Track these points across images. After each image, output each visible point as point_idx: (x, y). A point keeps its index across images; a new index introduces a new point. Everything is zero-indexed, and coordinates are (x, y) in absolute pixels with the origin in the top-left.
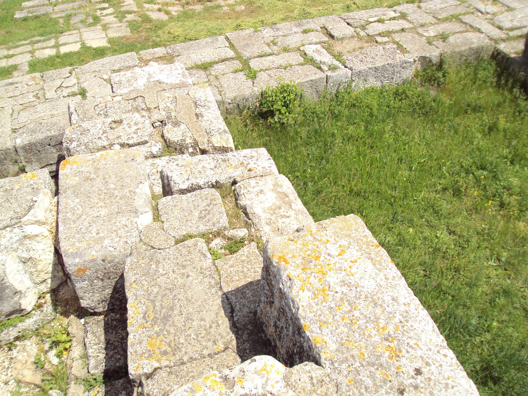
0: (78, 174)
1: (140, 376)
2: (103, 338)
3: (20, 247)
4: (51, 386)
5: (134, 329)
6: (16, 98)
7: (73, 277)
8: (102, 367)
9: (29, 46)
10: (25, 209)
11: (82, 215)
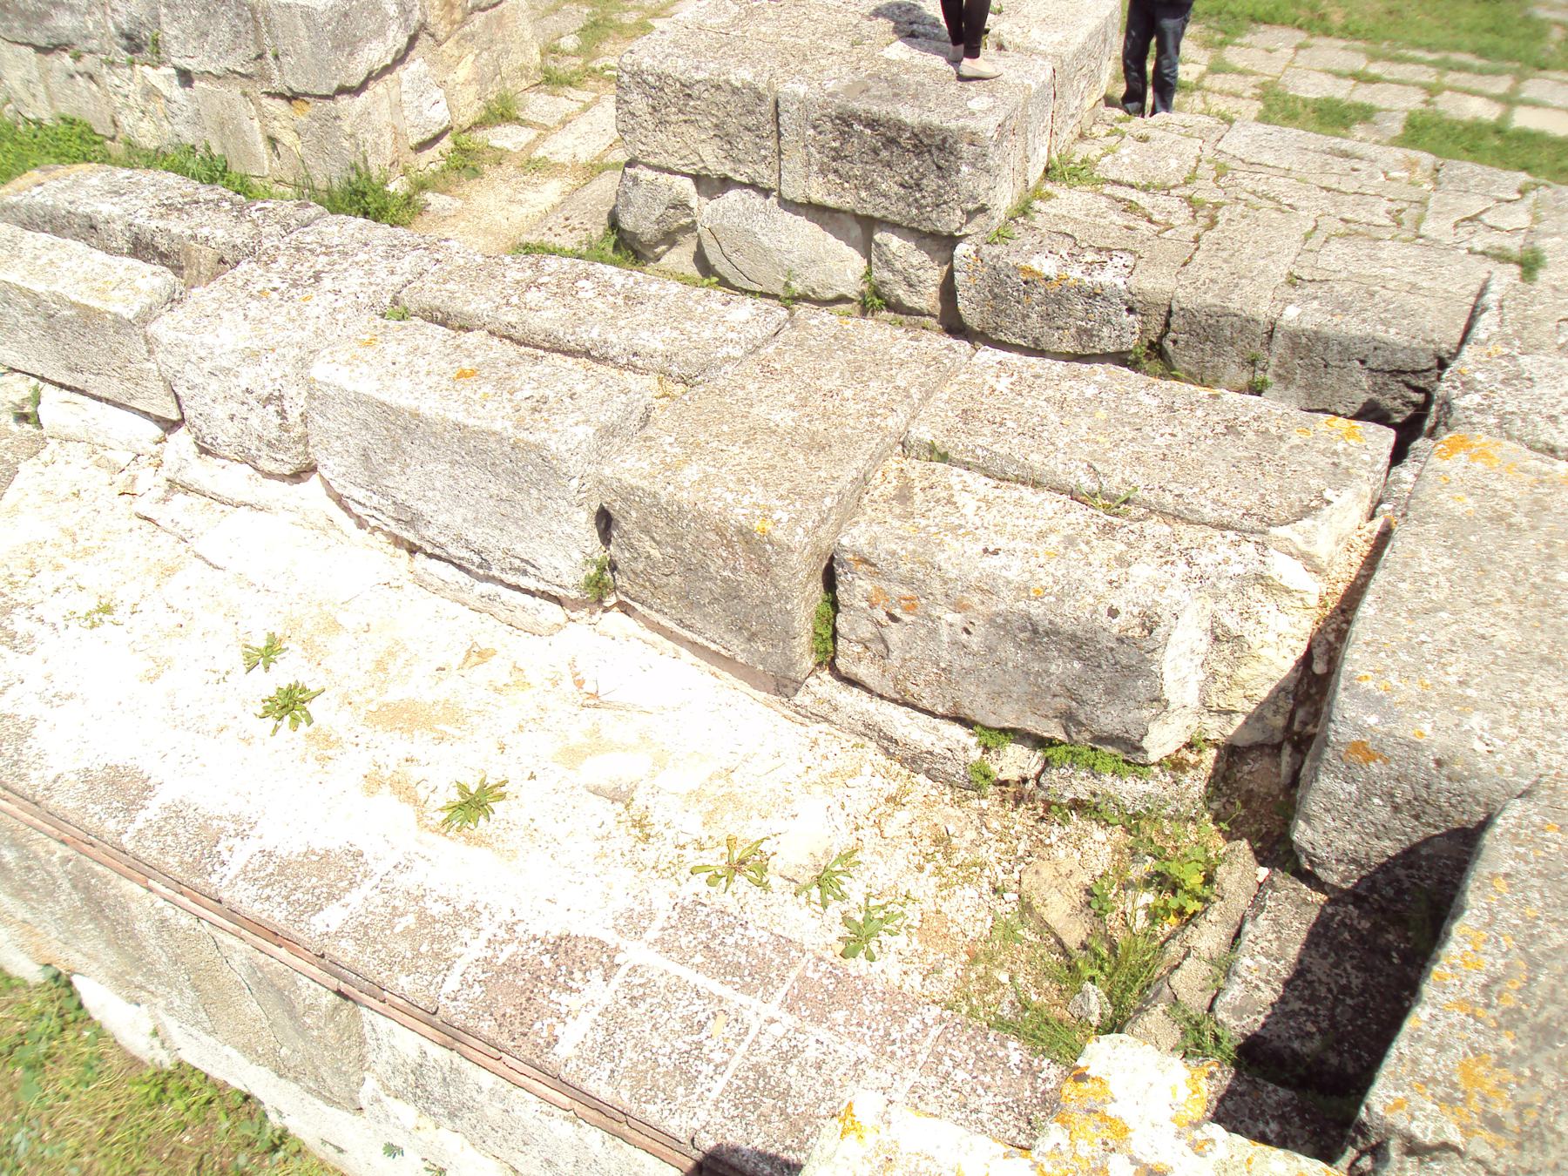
0: (1479, 492)
1: (1391, 1129)
2: (1293, 951)
3: (1231, 596)
4: (1096, 972)
5: (1441, 998)
6: (1340, 198)
7: (1329, 754)
8: (1253, 1023)
9: (1432, 71)
10: (1291, 506)
11: (1443, 609)
